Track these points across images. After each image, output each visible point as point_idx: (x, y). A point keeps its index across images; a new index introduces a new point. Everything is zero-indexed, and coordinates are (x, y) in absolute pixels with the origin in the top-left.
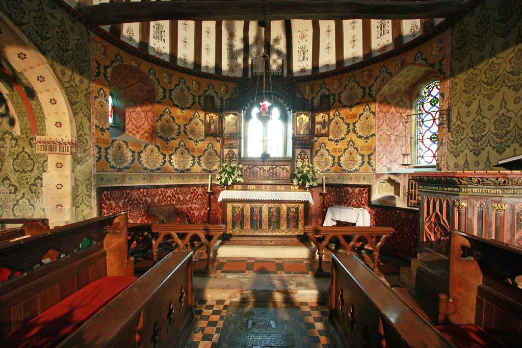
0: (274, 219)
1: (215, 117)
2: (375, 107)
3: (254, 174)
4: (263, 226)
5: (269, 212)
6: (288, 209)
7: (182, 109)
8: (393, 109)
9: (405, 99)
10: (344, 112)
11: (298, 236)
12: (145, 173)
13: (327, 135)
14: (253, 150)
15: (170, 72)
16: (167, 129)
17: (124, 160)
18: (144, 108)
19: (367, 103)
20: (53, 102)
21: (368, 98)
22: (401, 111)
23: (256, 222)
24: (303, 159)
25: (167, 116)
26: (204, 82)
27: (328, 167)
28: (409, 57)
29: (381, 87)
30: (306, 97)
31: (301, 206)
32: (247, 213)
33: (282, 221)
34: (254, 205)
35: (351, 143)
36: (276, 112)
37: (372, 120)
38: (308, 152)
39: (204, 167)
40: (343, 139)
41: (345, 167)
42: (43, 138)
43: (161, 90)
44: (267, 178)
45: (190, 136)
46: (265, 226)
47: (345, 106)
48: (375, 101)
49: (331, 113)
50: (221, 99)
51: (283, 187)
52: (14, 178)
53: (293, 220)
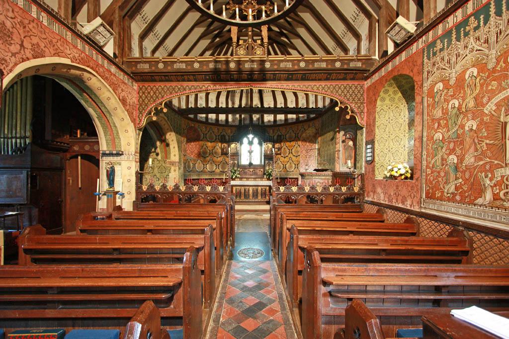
0: (255, 194)
1: (226, 145)
2: (300, 143)
3: (245, 173)
4: (250, 198)
6: (262, 189)
7: (211, 142)
8: (308, 144)
10: (288, 144)
12: (197, 173)
14: (244, 161)
15: (206, 125)
16: (205, 153)
17: (190, 168)
18: (195, 143)
19: (297, 141)
21: (297, 139)
22: (311, 144)
23: (246, 195)
25: (205, 146)
26: (221, 128)
27: (281, 170)
28: (311, 123)
29: (302, 134)
30: (271, 135)
31: (268, 188)
32: (243, 191)
33: (259, 195)
36: (256, 141)
38: (271, 162)
39: (221, 170)
40: (287, 156)
41: (288, 170)
42: (169, 160)
43: (202, 135)
45: (215, 155)
46: (251, 197)
47: (288, 141)
48: (300, 140)
49: (282, 144)
50: (229, 136)
51: (259, 179)
52: (158, 175)
53: (264, 194)
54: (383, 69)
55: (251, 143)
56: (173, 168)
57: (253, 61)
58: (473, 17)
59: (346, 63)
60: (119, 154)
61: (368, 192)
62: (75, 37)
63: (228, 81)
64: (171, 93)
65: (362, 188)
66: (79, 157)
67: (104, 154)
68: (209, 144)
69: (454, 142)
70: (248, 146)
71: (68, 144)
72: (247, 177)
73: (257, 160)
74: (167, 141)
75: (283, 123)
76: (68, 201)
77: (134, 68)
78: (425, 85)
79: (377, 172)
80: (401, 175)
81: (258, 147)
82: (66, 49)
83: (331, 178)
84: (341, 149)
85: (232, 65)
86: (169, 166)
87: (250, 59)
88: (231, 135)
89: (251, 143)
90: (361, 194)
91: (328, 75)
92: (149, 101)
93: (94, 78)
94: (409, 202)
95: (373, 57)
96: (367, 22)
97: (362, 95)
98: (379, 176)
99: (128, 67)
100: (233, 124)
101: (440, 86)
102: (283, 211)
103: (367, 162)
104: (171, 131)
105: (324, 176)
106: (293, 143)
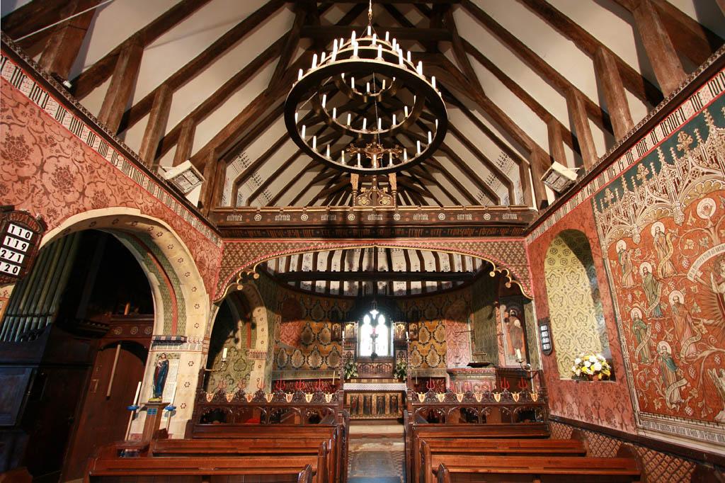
0: (381, 406)
1: (338, 326)
2: (445, 322)
4: (373, 411)
5: (377, 400)
6: (391, 397)
7: (317, 322)
8: (456, 324)
9: (463, 317)
10: (428, 324)
11: (398, 419)
13: (417, 339)
14: (365, 351)
16: (307, 338)
20: (263, 330)
21: (440, 316)
23: (367, 408)
24: (401, 358)
25: (308, 328)
27: (419, 364)
30: (403, 310)
31: (400, 395)
32: (362, 401)
33: (386, 407)
36: (382, 319)
37: (443, 331)
38: (405, 352)
39: (329, 365)
40: (427, 343)
41: (429, 364)
42: (253, 350)
46: (374, 411)
47: (428, 320)
48: (444, 318)
50: (343, 313)
51: (387, 380)
55: (374, 323)
56: (257, 362)
57: (378, 213)
59: (497, 215)
60: (179, 342)
61: (554, 402)
65: (543, 395)
66: (119, 346)
68: (314, 325)
69: (660, 321)
70: (371, 327)
71: (107, 325)
72: (369, 376)
73: (383, 350)
75: (420, 292)
77: (222, 221)
79: (561, 369)
80: (597, 373)
83: (494, 377)
84: (504, 331)
85: (351, 218)
89: (374, 323)
91: (476, 229)
93: (166, 234)
94: (617, 419)
95: (530, 208)
96: (516, 167)
100: (350, 295)
103: (544, 351)
104: (261, 305)
105: (484, 374)
106: (435, 323)
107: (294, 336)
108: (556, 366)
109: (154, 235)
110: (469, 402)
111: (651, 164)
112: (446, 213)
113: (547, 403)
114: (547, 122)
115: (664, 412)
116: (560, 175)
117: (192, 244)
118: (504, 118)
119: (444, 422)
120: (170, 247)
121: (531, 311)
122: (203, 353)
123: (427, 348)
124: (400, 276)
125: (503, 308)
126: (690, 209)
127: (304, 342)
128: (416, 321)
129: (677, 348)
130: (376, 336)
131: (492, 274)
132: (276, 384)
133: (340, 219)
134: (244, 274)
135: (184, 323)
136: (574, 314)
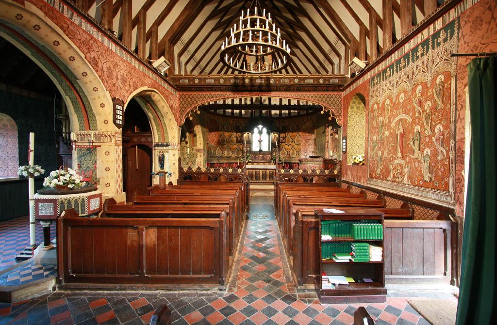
1: (240, 134)
2: (301, 133)
6: (270, 172)
8: (307, 134)
10: (291, 134)
13: (285, 142)
14: (255, 148)
16: (223, 141)
19: (298, 131)
20: (200, 137)
21: (298, 130)
23: (257, 177)
25: (223, 136)
30: (277, 126)
32: (254, 174)
34: (256, 170)
35: (293, 146)
36: (265, 130)
44: (261, 160)
47: (291, 132)
48: (300, 131)
50: (242, 127)
51: (268, 164)
54: (388, 59)
55: (260, 132)
56: (199, 154)
57: (261, 78)
58: (443, 30)
59: (327, 80)
60: (167, 145)
61: (344, 174)
62: (89, 25)
63: (244, 91)
64: (203, 100)
65: (340, 171)
66: (137, 147)
67: (157, 145)
68: (226, 134)
69: (381, 143)
70: (258, 135)
71: (129, 137)
72: (258, 161)
73: (265, 147)
74: (195, 133)
75: (287, 116)
76: (130, 179)
77: (178, 83)
78: (370, 104)
79: (348, 160)
80: (360, 162)
81: (267, 135)
82: (77, 34)
83: (322, 163)
84: (330, 140)
85: (247, 81)
86: (196, 152)
87: (259, 76)
88: (244, 126)
89: (260, 132)
90: (339, 175)
91: (315, 88)
92: (187, 105)
93: (157, 95)
94: (362, 181)
95: (346, 76)
96: (343, 47)
97: (340, 102)
98: (350, 163)
99: (173, 82)
100: (246, 116)
101: (388, 101)
102: (289, 194)
103: (343, 152)
104: (198, 124)
105: (317, 162)
106: (295, 134)
107: (216, 140)
108: (346, 159)
109: (152, 96)
110: (305, 174)
111: (449, 31)
112: (299, 78)
113: (341, 175)
114: (360, 25)
115: (375, 178)
116: (357, 65)
117: (167, 97)
118: (337, 18)
119: (292, 182)
120: (159, 101)
121: (341, 132)
122: (179, 150)
123: (290, 147)
124: (275, 107)
125: (330, 128)
126: (397, 97)
127: (221, 143)
128: (285, 132)
129: (383, 154)
130: (262, 141)
131: (322, 112)
132: (211, 165)
133: (241, 82)
134: (192, 111)
135: (168, 136)
136: (358, 135)
